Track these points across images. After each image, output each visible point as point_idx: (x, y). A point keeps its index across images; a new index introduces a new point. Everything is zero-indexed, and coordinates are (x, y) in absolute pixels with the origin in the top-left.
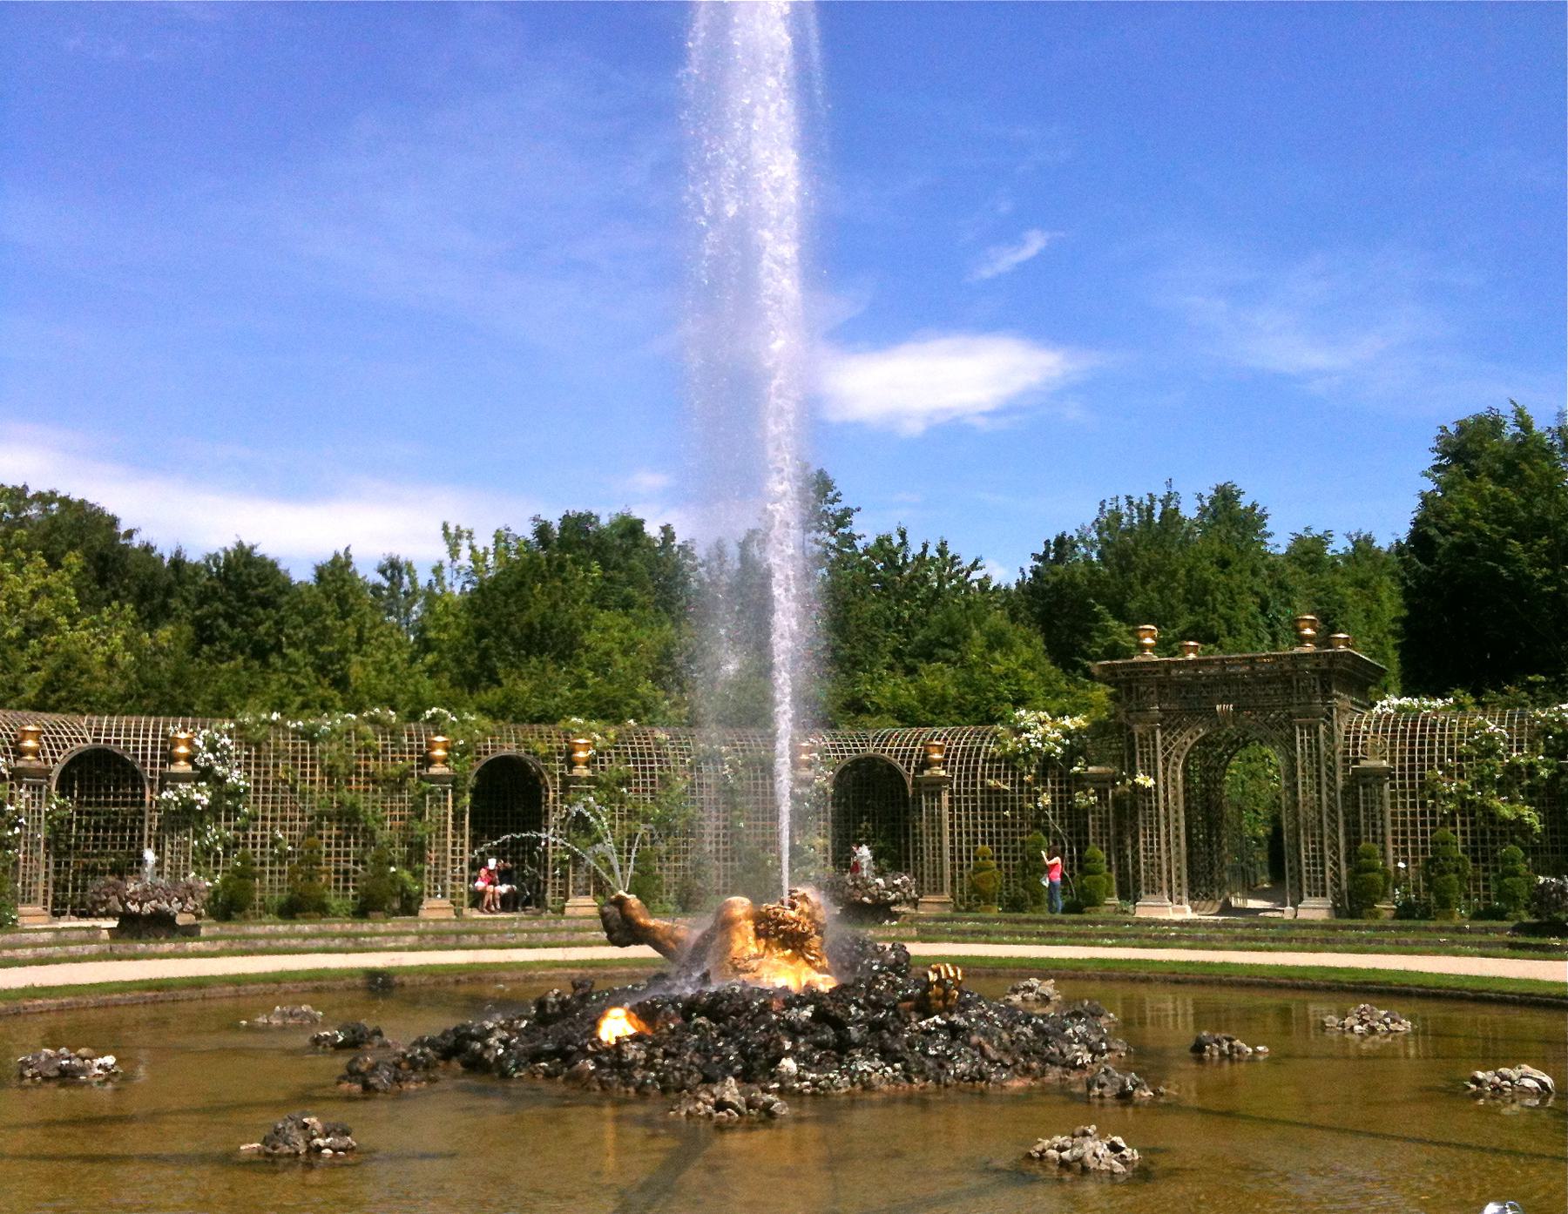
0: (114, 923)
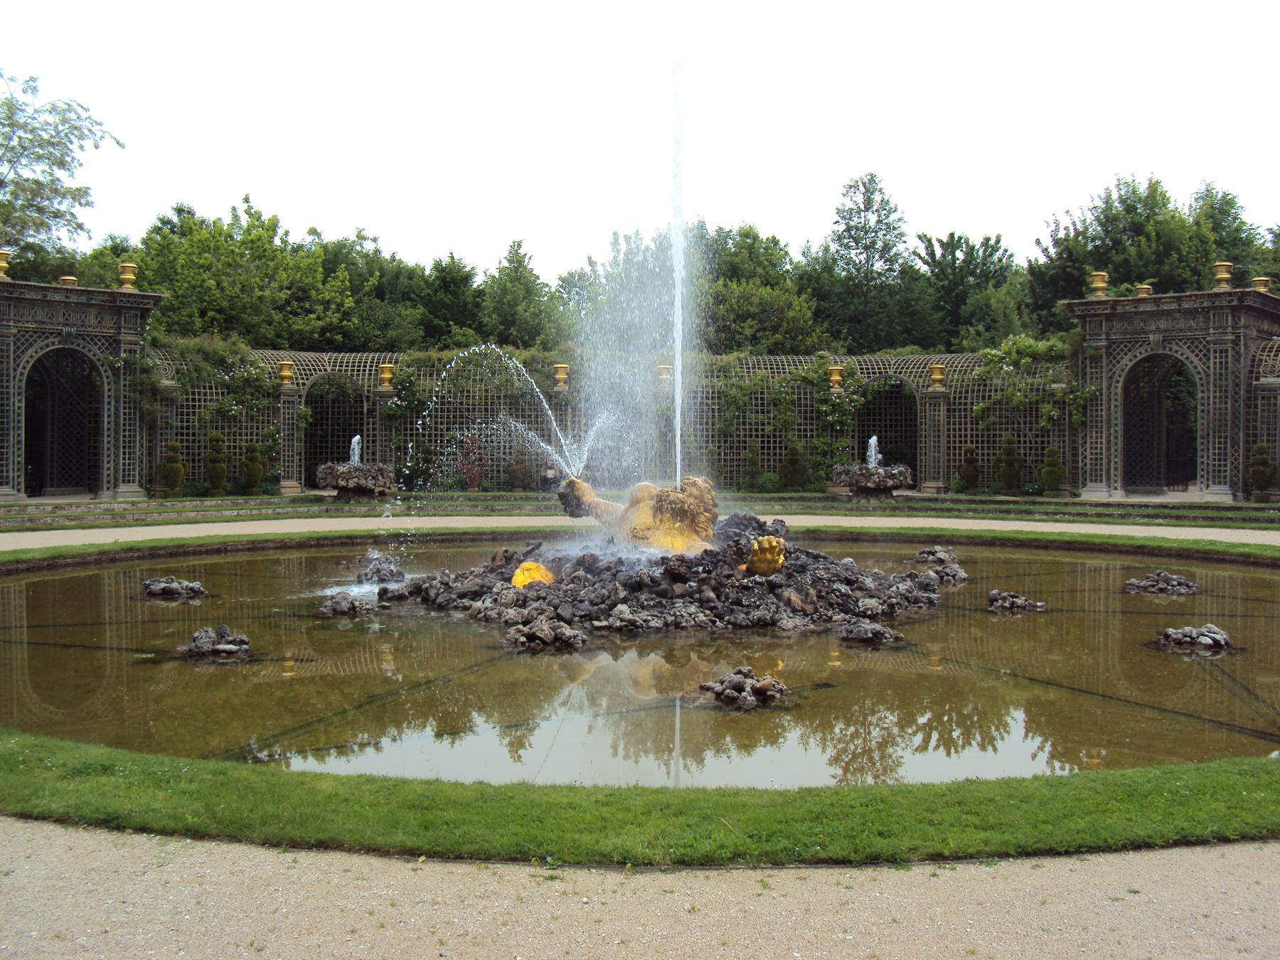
0: (335, 493)
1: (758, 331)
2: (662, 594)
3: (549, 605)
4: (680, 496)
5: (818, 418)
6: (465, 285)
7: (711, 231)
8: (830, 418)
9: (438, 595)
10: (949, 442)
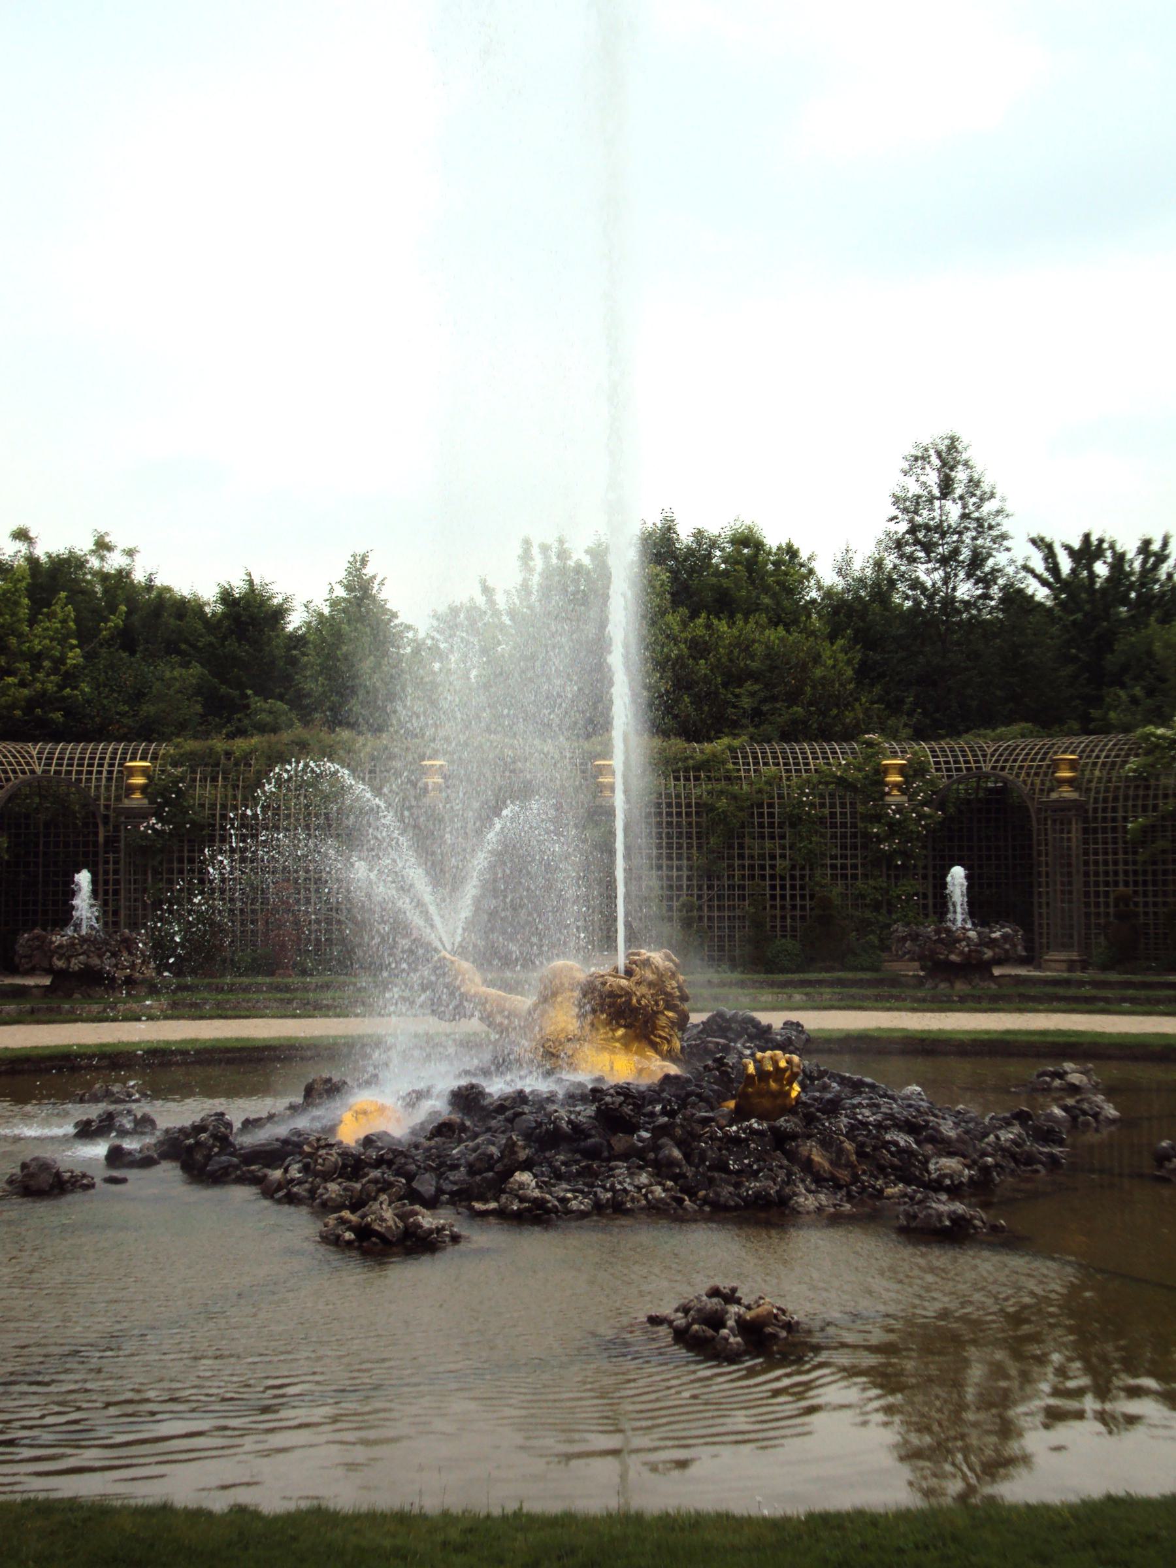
0: (47, 981)
1: (764, 701)
2: (592, 1154)
3: (398, 1173)
4: (624, 982)
5: (865, 847)
6: (273, 629)
7: (684, 536)
8: (885, 847)
9: (209, 1157)
10: (1086, 884)
